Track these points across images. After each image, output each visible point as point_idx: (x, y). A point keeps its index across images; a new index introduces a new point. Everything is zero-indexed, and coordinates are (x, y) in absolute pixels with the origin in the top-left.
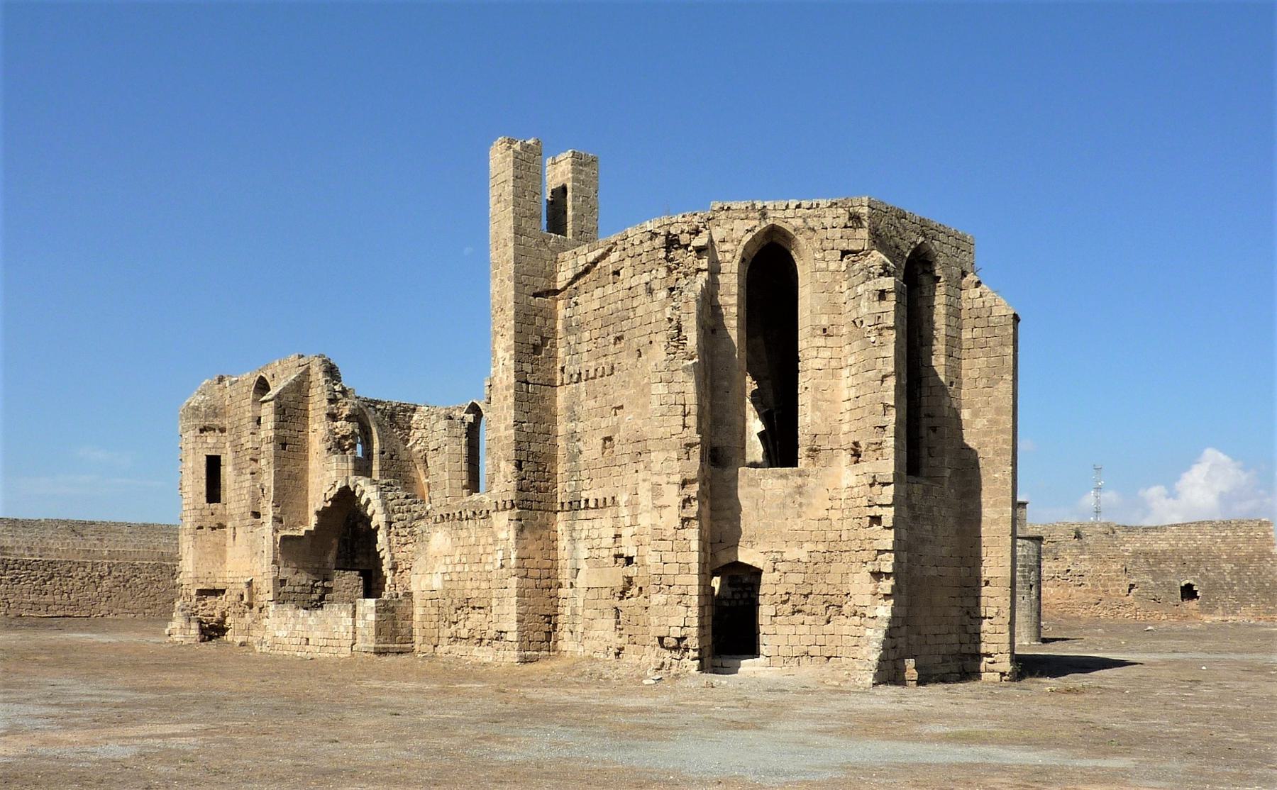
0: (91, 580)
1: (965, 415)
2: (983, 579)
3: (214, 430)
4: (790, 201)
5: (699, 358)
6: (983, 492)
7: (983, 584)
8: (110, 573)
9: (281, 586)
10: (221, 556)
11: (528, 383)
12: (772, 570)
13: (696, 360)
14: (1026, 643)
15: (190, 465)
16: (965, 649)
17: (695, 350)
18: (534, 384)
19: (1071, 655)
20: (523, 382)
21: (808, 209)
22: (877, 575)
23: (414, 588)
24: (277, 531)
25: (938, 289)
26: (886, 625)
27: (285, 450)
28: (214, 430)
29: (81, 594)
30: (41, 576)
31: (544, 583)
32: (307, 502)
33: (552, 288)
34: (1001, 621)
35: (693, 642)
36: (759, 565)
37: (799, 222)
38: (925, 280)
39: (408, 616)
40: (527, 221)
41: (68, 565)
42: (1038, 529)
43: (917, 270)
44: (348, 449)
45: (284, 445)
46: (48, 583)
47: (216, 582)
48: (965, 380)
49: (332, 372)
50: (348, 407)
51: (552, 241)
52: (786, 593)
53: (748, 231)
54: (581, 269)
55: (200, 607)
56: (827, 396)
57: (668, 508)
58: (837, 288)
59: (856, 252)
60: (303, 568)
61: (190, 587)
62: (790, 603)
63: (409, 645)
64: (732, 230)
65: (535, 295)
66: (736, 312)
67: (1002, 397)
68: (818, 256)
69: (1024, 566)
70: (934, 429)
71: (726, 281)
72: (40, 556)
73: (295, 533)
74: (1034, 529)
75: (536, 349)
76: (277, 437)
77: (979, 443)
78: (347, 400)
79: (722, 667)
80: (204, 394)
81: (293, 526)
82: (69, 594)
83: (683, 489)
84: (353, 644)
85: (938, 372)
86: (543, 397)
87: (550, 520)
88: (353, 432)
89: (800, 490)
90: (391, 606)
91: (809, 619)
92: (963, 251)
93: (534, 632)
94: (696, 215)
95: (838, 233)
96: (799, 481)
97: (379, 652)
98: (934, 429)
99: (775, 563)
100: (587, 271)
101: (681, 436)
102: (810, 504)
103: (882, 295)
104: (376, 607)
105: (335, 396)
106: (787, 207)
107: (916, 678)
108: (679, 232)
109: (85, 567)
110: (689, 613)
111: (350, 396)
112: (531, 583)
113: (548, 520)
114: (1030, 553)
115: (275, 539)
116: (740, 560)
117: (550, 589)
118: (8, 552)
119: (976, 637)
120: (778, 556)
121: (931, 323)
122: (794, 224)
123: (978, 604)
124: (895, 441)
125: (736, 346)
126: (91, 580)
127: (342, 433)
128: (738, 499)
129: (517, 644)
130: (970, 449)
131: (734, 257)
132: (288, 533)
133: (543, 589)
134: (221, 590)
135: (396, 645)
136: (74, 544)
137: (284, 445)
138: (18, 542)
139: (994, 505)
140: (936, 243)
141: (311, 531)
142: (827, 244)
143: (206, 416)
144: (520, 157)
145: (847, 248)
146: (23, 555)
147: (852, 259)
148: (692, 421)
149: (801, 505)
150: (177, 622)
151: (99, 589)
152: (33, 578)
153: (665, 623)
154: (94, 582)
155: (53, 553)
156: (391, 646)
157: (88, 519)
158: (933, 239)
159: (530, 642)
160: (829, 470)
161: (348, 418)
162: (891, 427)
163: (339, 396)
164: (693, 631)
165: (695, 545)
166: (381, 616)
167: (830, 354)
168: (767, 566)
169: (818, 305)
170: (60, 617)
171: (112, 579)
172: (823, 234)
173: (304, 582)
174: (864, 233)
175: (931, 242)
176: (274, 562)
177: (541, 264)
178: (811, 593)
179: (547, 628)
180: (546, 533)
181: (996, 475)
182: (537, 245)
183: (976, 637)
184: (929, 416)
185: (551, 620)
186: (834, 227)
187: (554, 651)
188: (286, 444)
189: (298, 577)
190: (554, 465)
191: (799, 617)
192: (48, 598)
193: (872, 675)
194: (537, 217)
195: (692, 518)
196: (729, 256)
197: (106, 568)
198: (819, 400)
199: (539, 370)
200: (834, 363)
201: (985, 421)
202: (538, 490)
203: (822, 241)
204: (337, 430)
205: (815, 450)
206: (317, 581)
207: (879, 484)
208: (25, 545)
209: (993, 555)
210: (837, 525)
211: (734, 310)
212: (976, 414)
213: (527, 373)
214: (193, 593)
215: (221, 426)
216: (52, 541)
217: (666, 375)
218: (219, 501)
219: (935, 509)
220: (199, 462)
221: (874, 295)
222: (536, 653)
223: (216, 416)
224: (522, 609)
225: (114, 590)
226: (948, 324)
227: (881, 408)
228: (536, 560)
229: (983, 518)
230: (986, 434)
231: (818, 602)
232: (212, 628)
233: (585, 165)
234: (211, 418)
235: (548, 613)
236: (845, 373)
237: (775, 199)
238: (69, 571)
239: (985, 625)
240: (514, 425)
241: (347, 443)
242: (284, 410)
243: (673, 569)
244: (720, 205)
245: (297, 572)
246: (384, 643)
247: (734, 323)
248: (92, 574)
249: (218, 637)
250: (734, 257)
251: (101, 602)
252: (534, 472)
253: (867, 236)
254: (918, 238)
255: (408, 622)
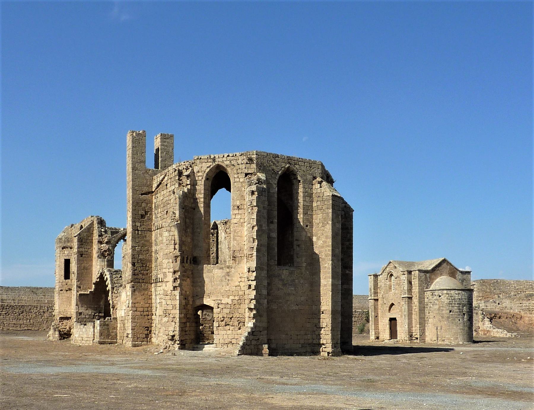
0: (40, 313)
1: (314, 239)
2: (321, 311)
3: (68, 248)
4: (225, 154)
5: (180, 221)
6: (321, 273)
7: (321, 313)
8: (48, 310)
9: (80, 315)
10: (69, 302)
11: (138, 230)
12: (217, 308)
13: (179, 222)
14: (461, 343)
15: (58, 263)
16: (314, 342)
17: (178, 218)
18: (141, 231)
19: (443, 348)
20: (136, 230)
21: (232, 157)
22: (251, 309)
23: (118, 316)
24: (78, 292)
25: (300, 185)
26: (250, 330)
27: (82, 257)
28: (68, 248)
29: (35, 320)
30: (18, 312)
31: (145, 313)
32: (92, 279)
33: (150, 191)
34: (328, 329)
35: (177, 337)
36: (212, 305)
37: (228, 162)
38: (295, 182)
39: (115, 328)
40: (138, 165)
41: (30, 307)
42: (530, 283)
43: (291, 177)
44: (107, 256)
45: (82, 255)
46: (21, 315)
47: (67, 314)
48: (314, 224)
49: (101, 223)
50: (107, 238)
51: (150, 171)
52: (223, 317)
53: (208, 167)
54: (158, 183)
55: (60, 325)
56: (239, 234)
57: (169, 282)
58: (243, 189)
59: (251, 174)
60: (89, 307)
61: (57, 316)
62: (224, 321)
63: (115, 340)
64: (202, 167)
65: (142, 194)
66: (203, 201)
67: (327, 231)
68: (236, 176)
69: (460, 304)
70: (299, 246)
71: (199, 188)
72: (18, 303)
73: (86, 293)
74: (528, 283)
75: (143, 216)
76: (78, 252)
77: (319, 252)
78: (107, 235)
79: (197, 348)
80: (64, 233)
81: (85, 289)
82: (30, 320)
83: (174, 274)
84: (93, 340)
85: (300, 221)
86: (146, 236)
87: (148, 287)
88: (109, 249)
89: (228, 274)
90: (107, 323)
91: (232, 328)
92: (314, 168)
93: (140, 334)
94: (188, 162)
95: (244, 166)
96: (228, 270)
97: (101, 343)
98: (299, 246)
99: (218, 305)
100: (160, 183)
101: (173, 253)
102: (232, 280)
103: (253, 193)
104: (100, 324)
105: (101, 233)
106: (224, 156)
107: (268, 353)
108: (182, 169)
109: (37, 308)
110: (176, 326)
111: (108, 233)
112: (139, 313)
113: (147, 287)
114: (463, 297)
115: (77, 295)
116: (205, 303)
117: (148, 316)
118: (4, 301)
119: (319, 337)
120: (220, 302)
121: (298, 200)
122: (226, 163)
123: (319, 322)
124: (256, 253)
125: (203, 214)
126: (40, 313)
127: (104, 249)
128: (203, 278)
129: (132, 339)
130: (316, 254)
131: (202, 178)
132: (82, 293)
133: (144, 316)
134: (70, 317)
135: (109, 340)
136: (33, 297)
137: (82, 255)
138: (9, 297)
139: (325, 278)
140: (297, 166)
141: (92, 292)
142: (239, 171)
143: (65, 242)
144: (135, 139)
145: (247, 172)
146: (10, 303)
147: (250, 176)
148: (177, 247)
149: (228, 280)
150: (51, 332)
151: (43, 318)
152: (14, 313)
153: (167, 329)
154: (41, 314)
155: (24, 302)
156: (107, 340)
157: (39, 286)
158: (295, 165)
159: (138, 338)
160: (240, 265)
161: (107, 243)
162: (255, 248)
163: (103, 233)
164: (177, 333)
165: (178, 298)
166: (102, 328)
167: (240, 217)
168: (215, 306)
169: (236, 196)
170: (26, 330)
171: (49, 313)
172: (237, 167)
173: (90, 314)
174: (254, 166)
175: (294, 166)
176: (77, 305)
177: (145, 182)
178: (233, 317)
179: (146, 332)
180: (146, 292)
181: (326, 265)
182: (143, 174)
183: (318, 336)
184: (297, 240)
185: (148, 329)
186: (242, 164)
187: (150, 342)
188: (82, 255)
189: (87, 311)
190: (151, 264)
191: (228, 327)
192: (21, 322)
193: (238, 351)
194: (143, 162)
195: (177, 286)
196: (200, 178)
197: (46, 308)
198: (236, 236)
199: (144, 225)
200: (242, 221)
201: (322, 241)
202: (143, 274)
203: (237, 170)
204: (102, 248)
205: (235, 257)
206: (96, 313)
207: (251, 271)
208: (12, 298)
209: (325, 300)
210: (243, 289)
211: (202, 200)
212: (318, 239)
213: (138, 226)
214: (58, 318)
215: (70, 246)
216: (23, 296)
217: (168, 228)
218: (69, 279)
219: (296, 280)
220: (61, 262)
221: (250, 193)
222: (141, 343)
223: (68, 242)
224: (134, 325)
225: (49, 318)
226: (304, 200)
227: (252, 240)
228: (141, 304)
229: (321, 284)
230: (322, 247)
231: (235, 321)
232: (65, 334)
233: (167, 139)
234: (66, 243)
235: (147, 326)
236: (245, 224)
237: (218, 153)
238: (30, 310)
239: (322, 332)
240: (132, 248)
241: (106, 253)
242: (82, 240)
243: (170, 307)
244: (197, 157)
245: (87, 309)
246: (104, 339)
247: (202, 205)
248: (40, 311)
249: (68, 338)
250: (202, 178)
251: (44, 323)
252: (141, 267)
253: (255, 167)
254: (286, 165)
255: (115, 330)
